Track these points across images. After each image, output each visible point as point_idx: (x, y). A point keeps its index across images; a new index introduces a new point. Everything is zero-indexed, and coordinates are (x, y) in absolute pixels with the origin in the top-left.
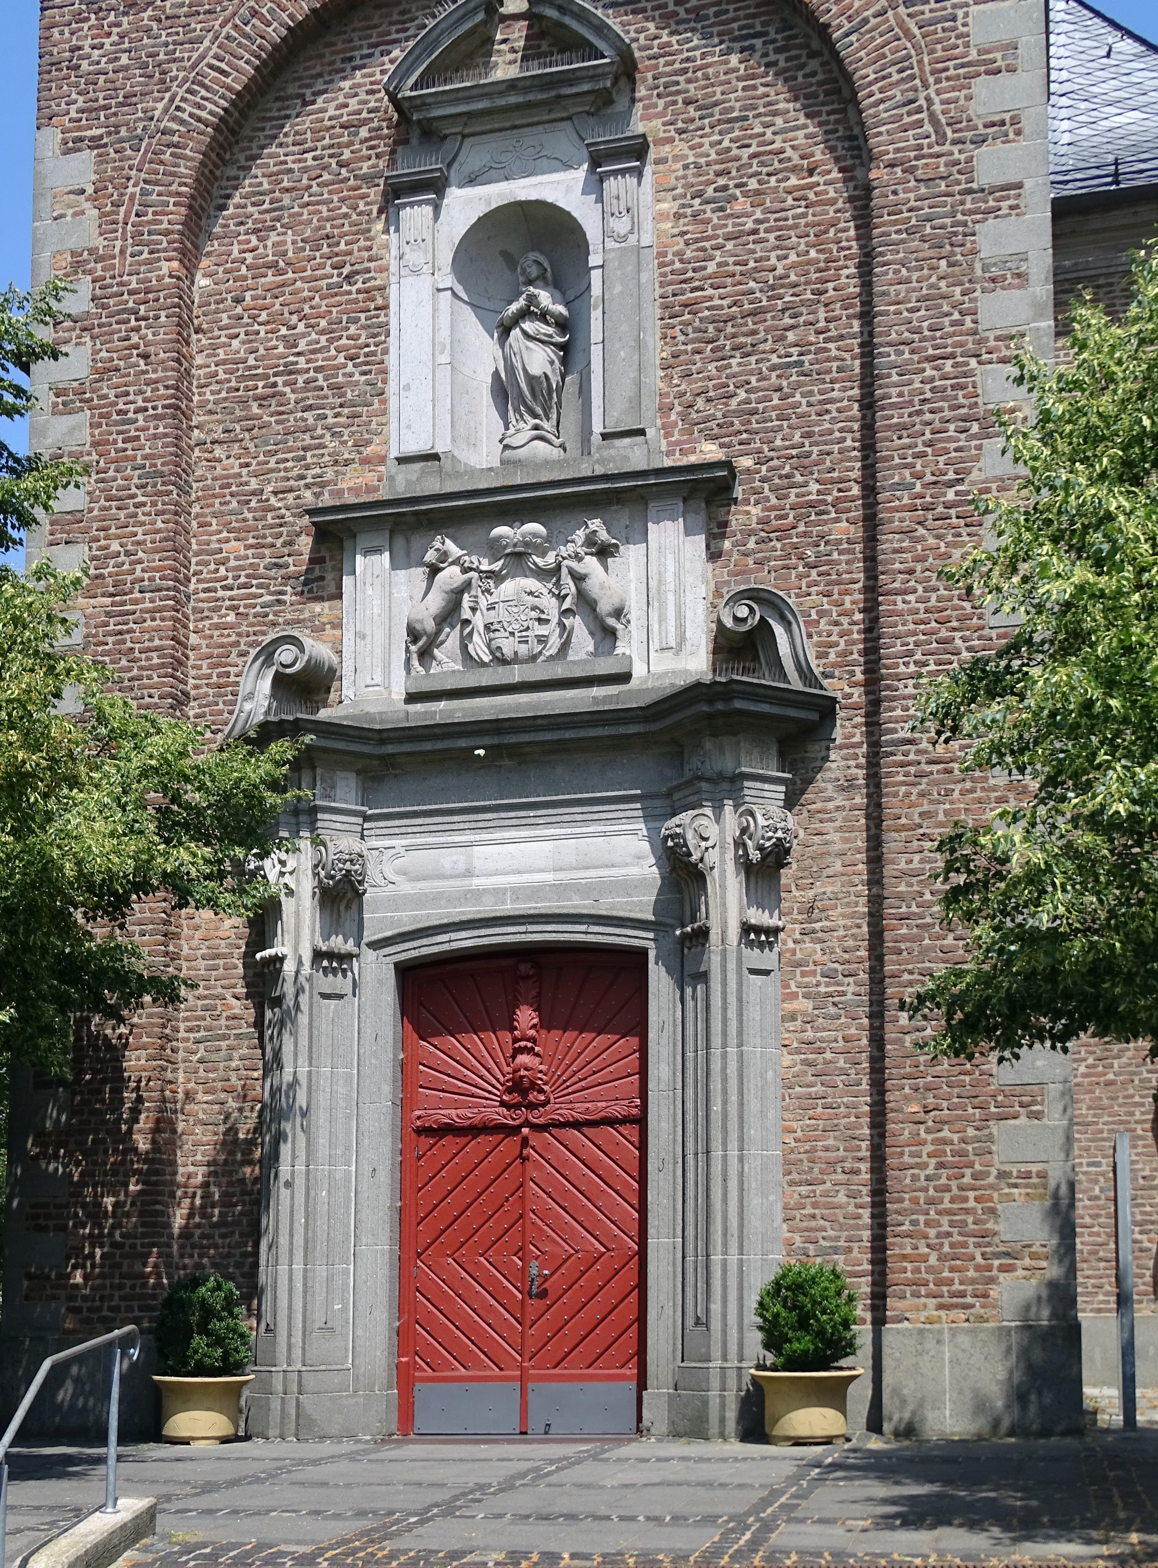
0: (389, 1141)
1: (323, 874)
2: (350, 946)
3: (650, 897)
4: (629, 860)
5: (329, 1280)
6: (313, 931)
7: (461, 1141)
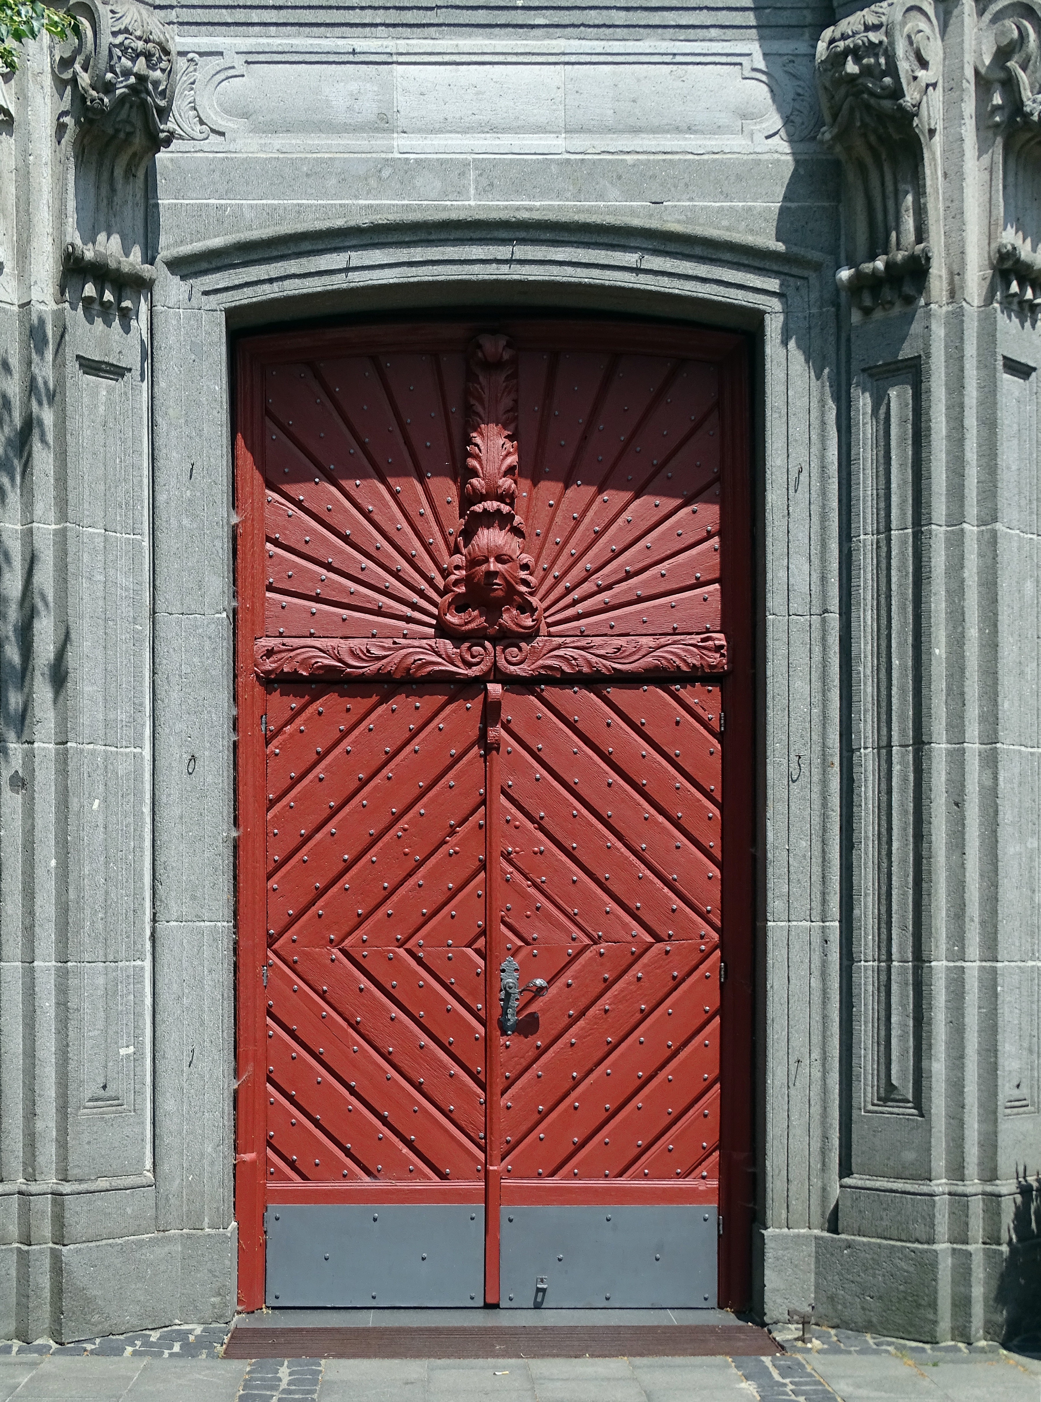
1: (85, 79)
2: (133, 261)
3: (769, 203)
4: (724, 119)
5: (110, 993)
6: (61, 215)
7: (358, 705)
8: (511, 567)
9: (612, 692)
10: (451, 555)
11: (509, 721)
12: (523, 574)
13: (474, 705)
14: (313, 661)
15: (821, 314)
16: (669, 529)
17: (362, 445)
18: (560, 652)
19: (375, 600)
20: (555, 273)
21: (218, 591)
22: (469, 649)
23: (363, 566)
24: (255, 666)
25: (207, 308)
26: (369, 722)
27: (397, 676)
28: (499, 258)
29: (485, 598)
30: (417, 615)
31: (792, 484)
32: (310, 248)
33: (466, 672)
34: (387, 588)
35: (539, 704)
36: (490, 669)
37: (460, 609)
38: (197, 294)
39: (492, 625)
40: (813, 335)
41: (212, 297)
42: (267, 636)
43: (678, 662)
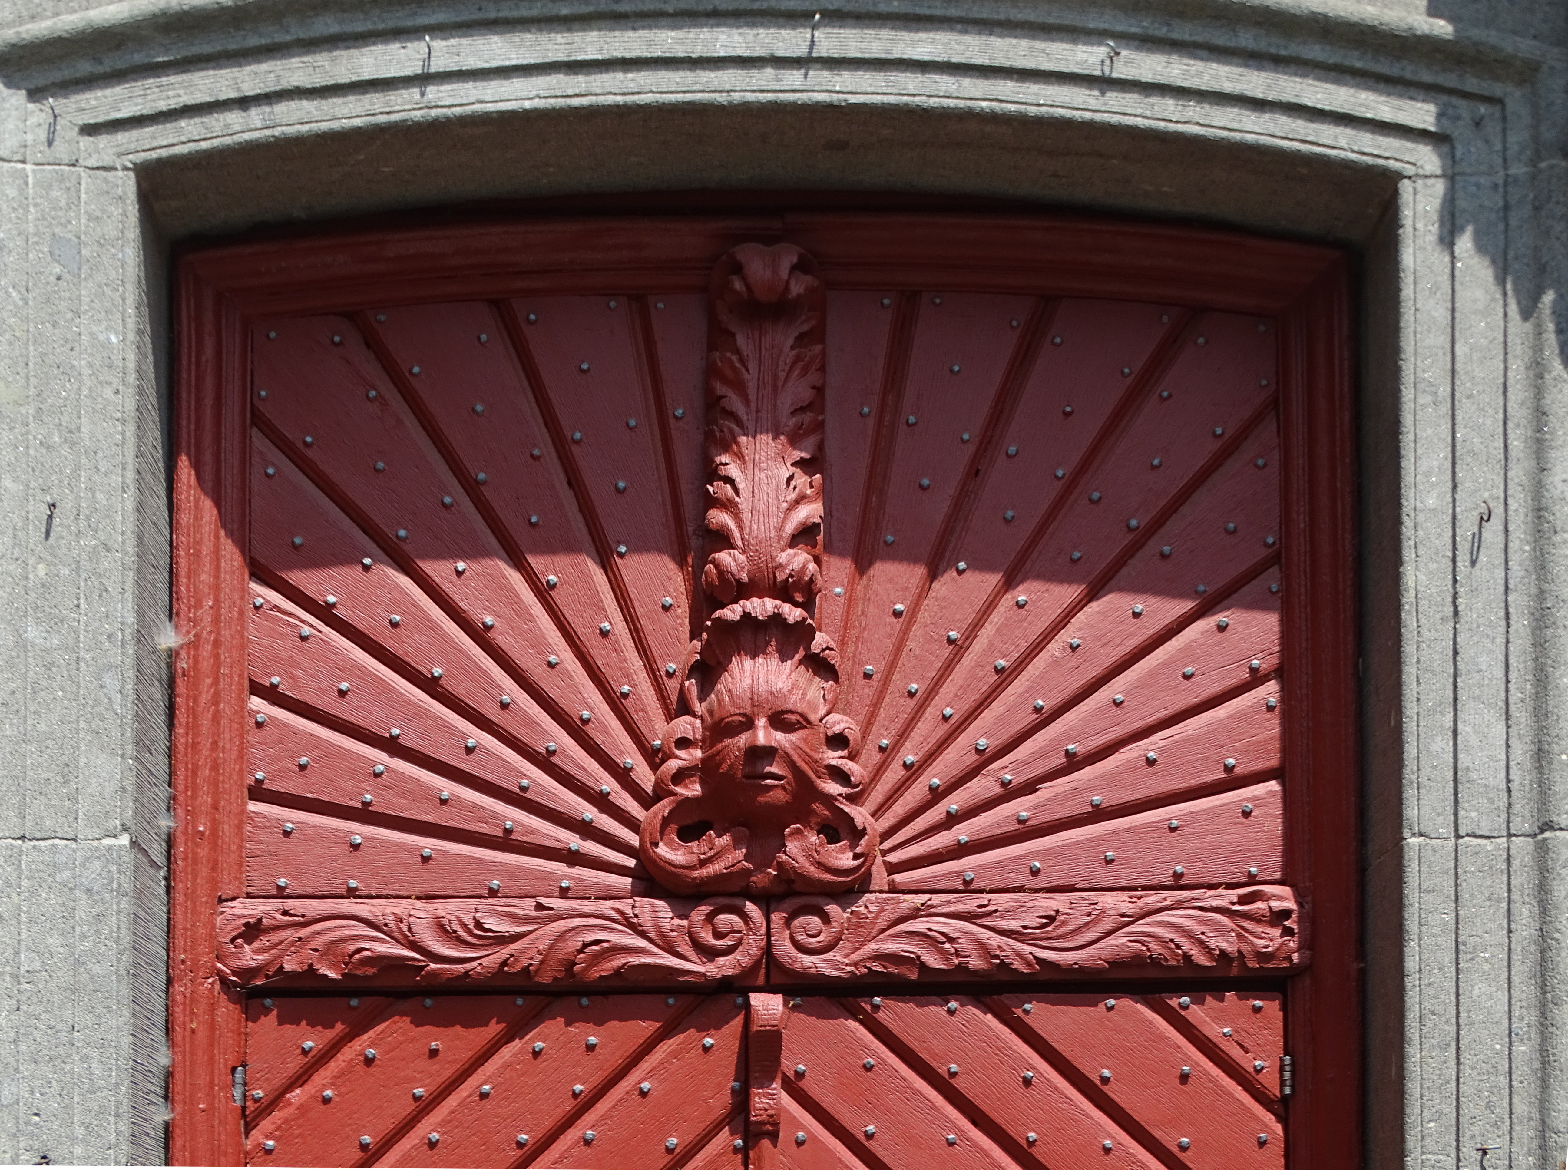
0: (118, 1025)
7: (455, 1042)
8: (805, 740)
9: (1036, 1012)
10: (670, 716)
11: (800, 1075)
12: (833, 757)
13: (722, 1041)
14: (352, 947)
15: (1533, 177)
16: (1165, 664)
17: (472, 488)
18: (919, 925)
19: (495, 815)
20: (911, 89)
21: (110, 788)
22: (710, 918)
23: (471, 743)
24: (219, 958)
25: (93, 162)
26: (482, 1080)
27: (546, 978)
28: (780, 53)
29: (747, 809)
30: (593, 848)
31: (1463, 548)
32: (335, 29)
33: (701, 969)
34: (524, 789)
35: (868, 1037)
36: (756, 965)
37: (688, 834)
38: (67, 132)
39: (761, 866)
40: (1514, 222)
41: (103, 140)
42: (249, 896)
43: (1187, 946)
